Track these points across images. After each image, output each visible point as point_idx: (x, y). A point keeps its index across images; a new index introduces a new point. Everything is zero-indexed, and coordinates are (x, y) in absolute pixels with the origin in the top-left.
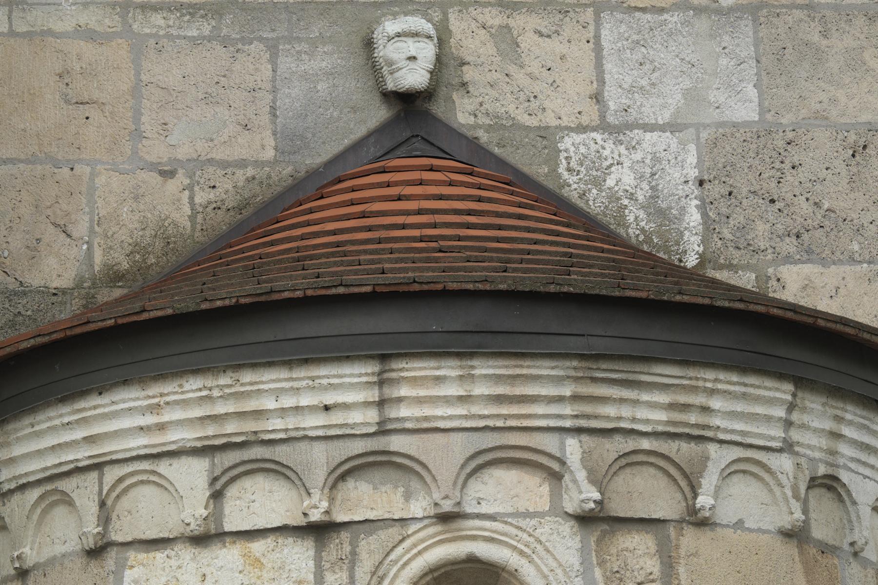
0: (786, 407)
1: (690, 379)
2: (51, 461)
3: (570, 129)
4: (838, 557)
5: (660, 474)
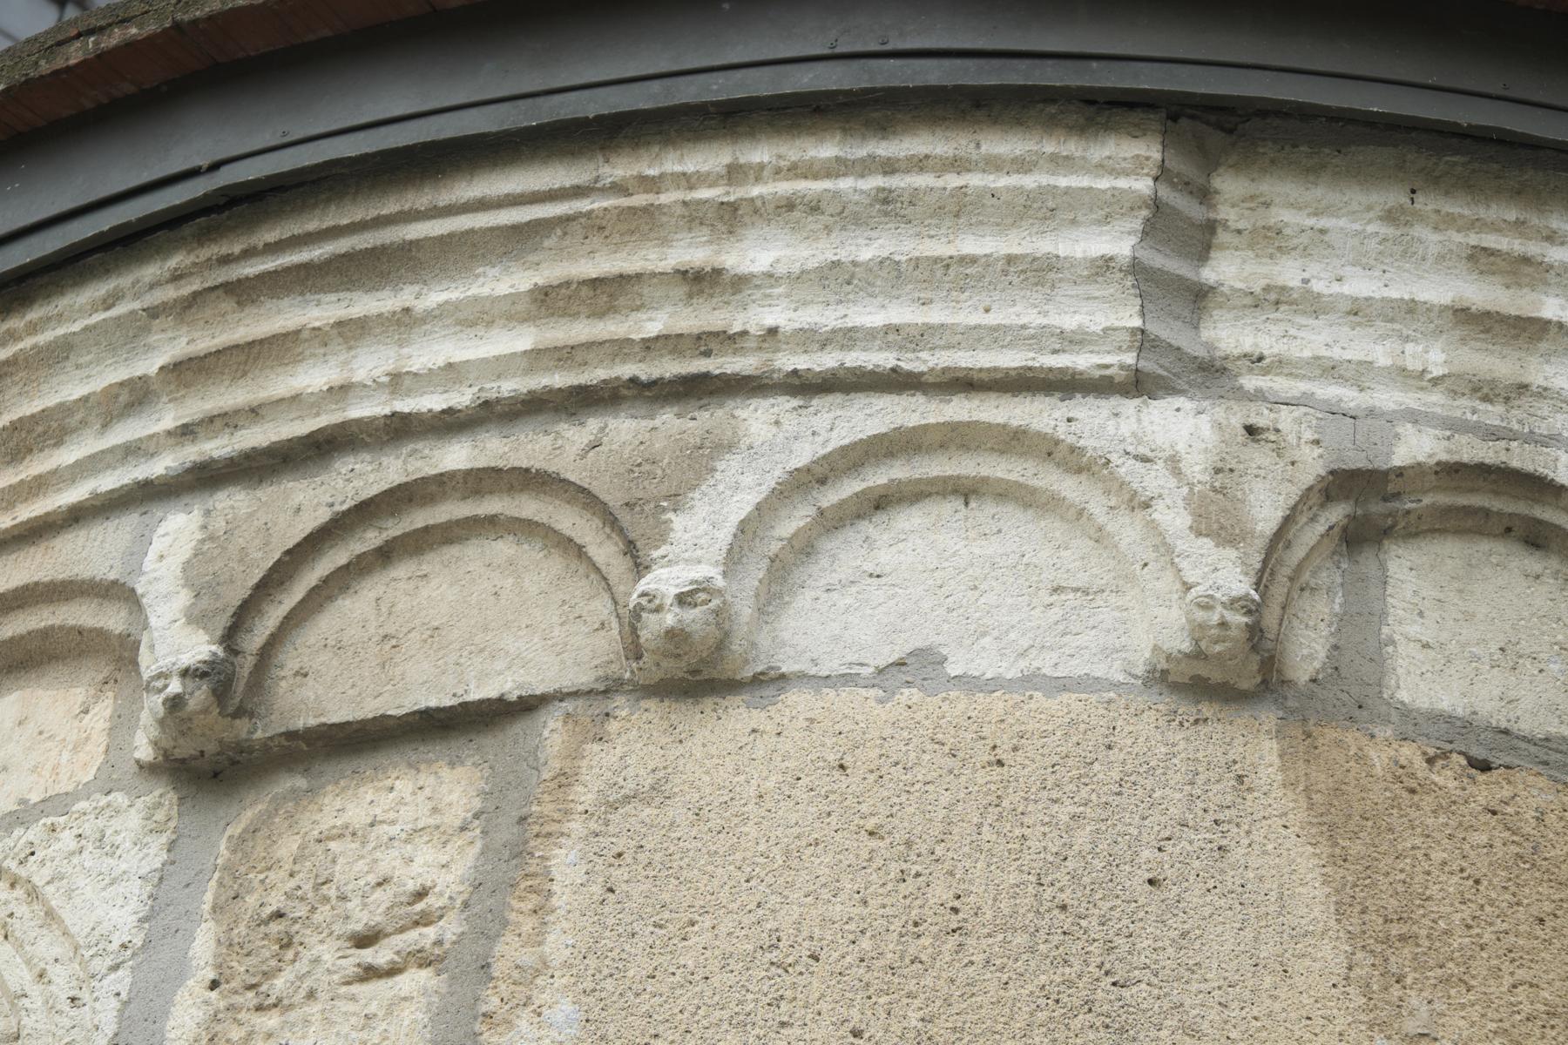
0: (1138, 224)
1: (619, 189)
5: (529, 552)
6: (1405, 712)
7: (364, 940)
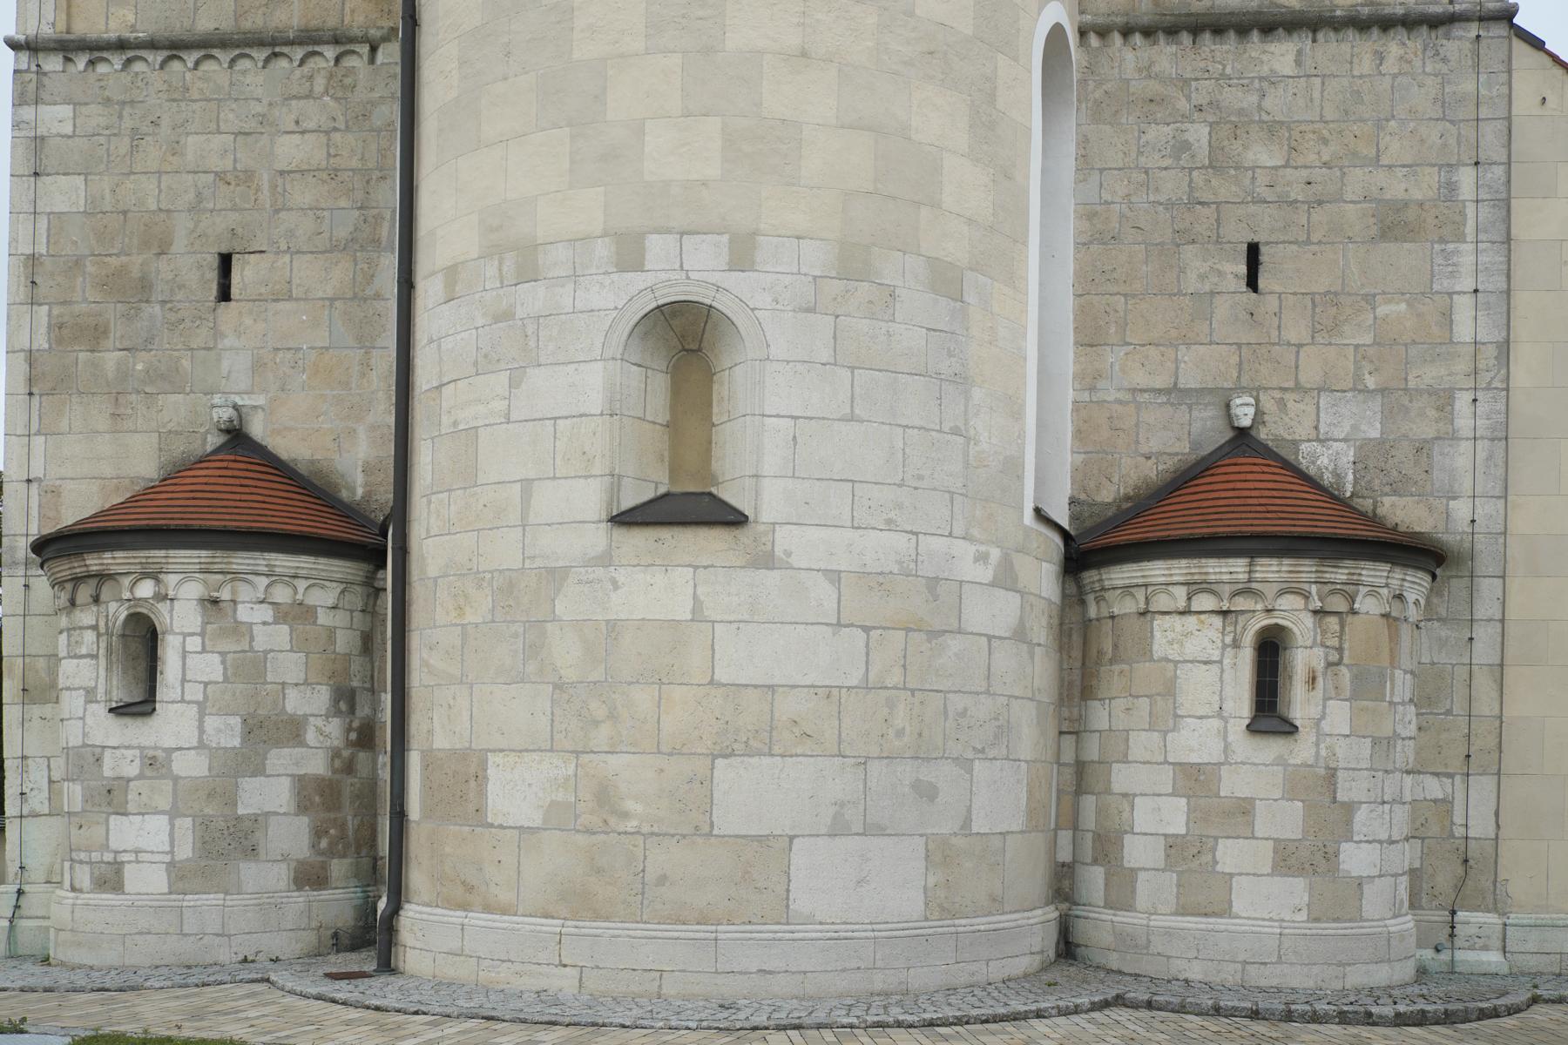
2: (1127, 581)
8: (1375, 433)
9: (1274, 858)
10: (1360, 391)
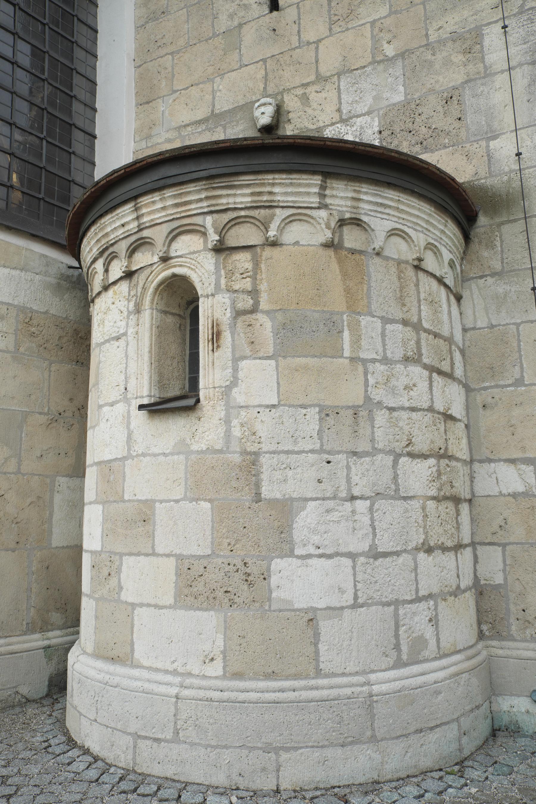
1: (260, 180)
3: (328, 125)
4: (364, 255)
5: (252, 226)
6: (346, 248)
7: (242, 274)
8: (399, 97)
9: (176, 583)
10: (379, 62)
